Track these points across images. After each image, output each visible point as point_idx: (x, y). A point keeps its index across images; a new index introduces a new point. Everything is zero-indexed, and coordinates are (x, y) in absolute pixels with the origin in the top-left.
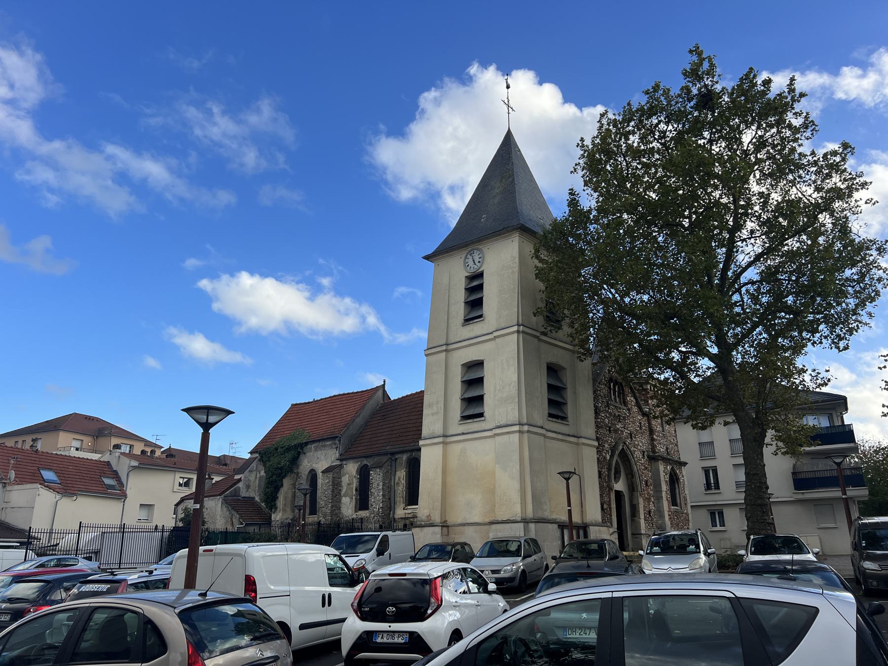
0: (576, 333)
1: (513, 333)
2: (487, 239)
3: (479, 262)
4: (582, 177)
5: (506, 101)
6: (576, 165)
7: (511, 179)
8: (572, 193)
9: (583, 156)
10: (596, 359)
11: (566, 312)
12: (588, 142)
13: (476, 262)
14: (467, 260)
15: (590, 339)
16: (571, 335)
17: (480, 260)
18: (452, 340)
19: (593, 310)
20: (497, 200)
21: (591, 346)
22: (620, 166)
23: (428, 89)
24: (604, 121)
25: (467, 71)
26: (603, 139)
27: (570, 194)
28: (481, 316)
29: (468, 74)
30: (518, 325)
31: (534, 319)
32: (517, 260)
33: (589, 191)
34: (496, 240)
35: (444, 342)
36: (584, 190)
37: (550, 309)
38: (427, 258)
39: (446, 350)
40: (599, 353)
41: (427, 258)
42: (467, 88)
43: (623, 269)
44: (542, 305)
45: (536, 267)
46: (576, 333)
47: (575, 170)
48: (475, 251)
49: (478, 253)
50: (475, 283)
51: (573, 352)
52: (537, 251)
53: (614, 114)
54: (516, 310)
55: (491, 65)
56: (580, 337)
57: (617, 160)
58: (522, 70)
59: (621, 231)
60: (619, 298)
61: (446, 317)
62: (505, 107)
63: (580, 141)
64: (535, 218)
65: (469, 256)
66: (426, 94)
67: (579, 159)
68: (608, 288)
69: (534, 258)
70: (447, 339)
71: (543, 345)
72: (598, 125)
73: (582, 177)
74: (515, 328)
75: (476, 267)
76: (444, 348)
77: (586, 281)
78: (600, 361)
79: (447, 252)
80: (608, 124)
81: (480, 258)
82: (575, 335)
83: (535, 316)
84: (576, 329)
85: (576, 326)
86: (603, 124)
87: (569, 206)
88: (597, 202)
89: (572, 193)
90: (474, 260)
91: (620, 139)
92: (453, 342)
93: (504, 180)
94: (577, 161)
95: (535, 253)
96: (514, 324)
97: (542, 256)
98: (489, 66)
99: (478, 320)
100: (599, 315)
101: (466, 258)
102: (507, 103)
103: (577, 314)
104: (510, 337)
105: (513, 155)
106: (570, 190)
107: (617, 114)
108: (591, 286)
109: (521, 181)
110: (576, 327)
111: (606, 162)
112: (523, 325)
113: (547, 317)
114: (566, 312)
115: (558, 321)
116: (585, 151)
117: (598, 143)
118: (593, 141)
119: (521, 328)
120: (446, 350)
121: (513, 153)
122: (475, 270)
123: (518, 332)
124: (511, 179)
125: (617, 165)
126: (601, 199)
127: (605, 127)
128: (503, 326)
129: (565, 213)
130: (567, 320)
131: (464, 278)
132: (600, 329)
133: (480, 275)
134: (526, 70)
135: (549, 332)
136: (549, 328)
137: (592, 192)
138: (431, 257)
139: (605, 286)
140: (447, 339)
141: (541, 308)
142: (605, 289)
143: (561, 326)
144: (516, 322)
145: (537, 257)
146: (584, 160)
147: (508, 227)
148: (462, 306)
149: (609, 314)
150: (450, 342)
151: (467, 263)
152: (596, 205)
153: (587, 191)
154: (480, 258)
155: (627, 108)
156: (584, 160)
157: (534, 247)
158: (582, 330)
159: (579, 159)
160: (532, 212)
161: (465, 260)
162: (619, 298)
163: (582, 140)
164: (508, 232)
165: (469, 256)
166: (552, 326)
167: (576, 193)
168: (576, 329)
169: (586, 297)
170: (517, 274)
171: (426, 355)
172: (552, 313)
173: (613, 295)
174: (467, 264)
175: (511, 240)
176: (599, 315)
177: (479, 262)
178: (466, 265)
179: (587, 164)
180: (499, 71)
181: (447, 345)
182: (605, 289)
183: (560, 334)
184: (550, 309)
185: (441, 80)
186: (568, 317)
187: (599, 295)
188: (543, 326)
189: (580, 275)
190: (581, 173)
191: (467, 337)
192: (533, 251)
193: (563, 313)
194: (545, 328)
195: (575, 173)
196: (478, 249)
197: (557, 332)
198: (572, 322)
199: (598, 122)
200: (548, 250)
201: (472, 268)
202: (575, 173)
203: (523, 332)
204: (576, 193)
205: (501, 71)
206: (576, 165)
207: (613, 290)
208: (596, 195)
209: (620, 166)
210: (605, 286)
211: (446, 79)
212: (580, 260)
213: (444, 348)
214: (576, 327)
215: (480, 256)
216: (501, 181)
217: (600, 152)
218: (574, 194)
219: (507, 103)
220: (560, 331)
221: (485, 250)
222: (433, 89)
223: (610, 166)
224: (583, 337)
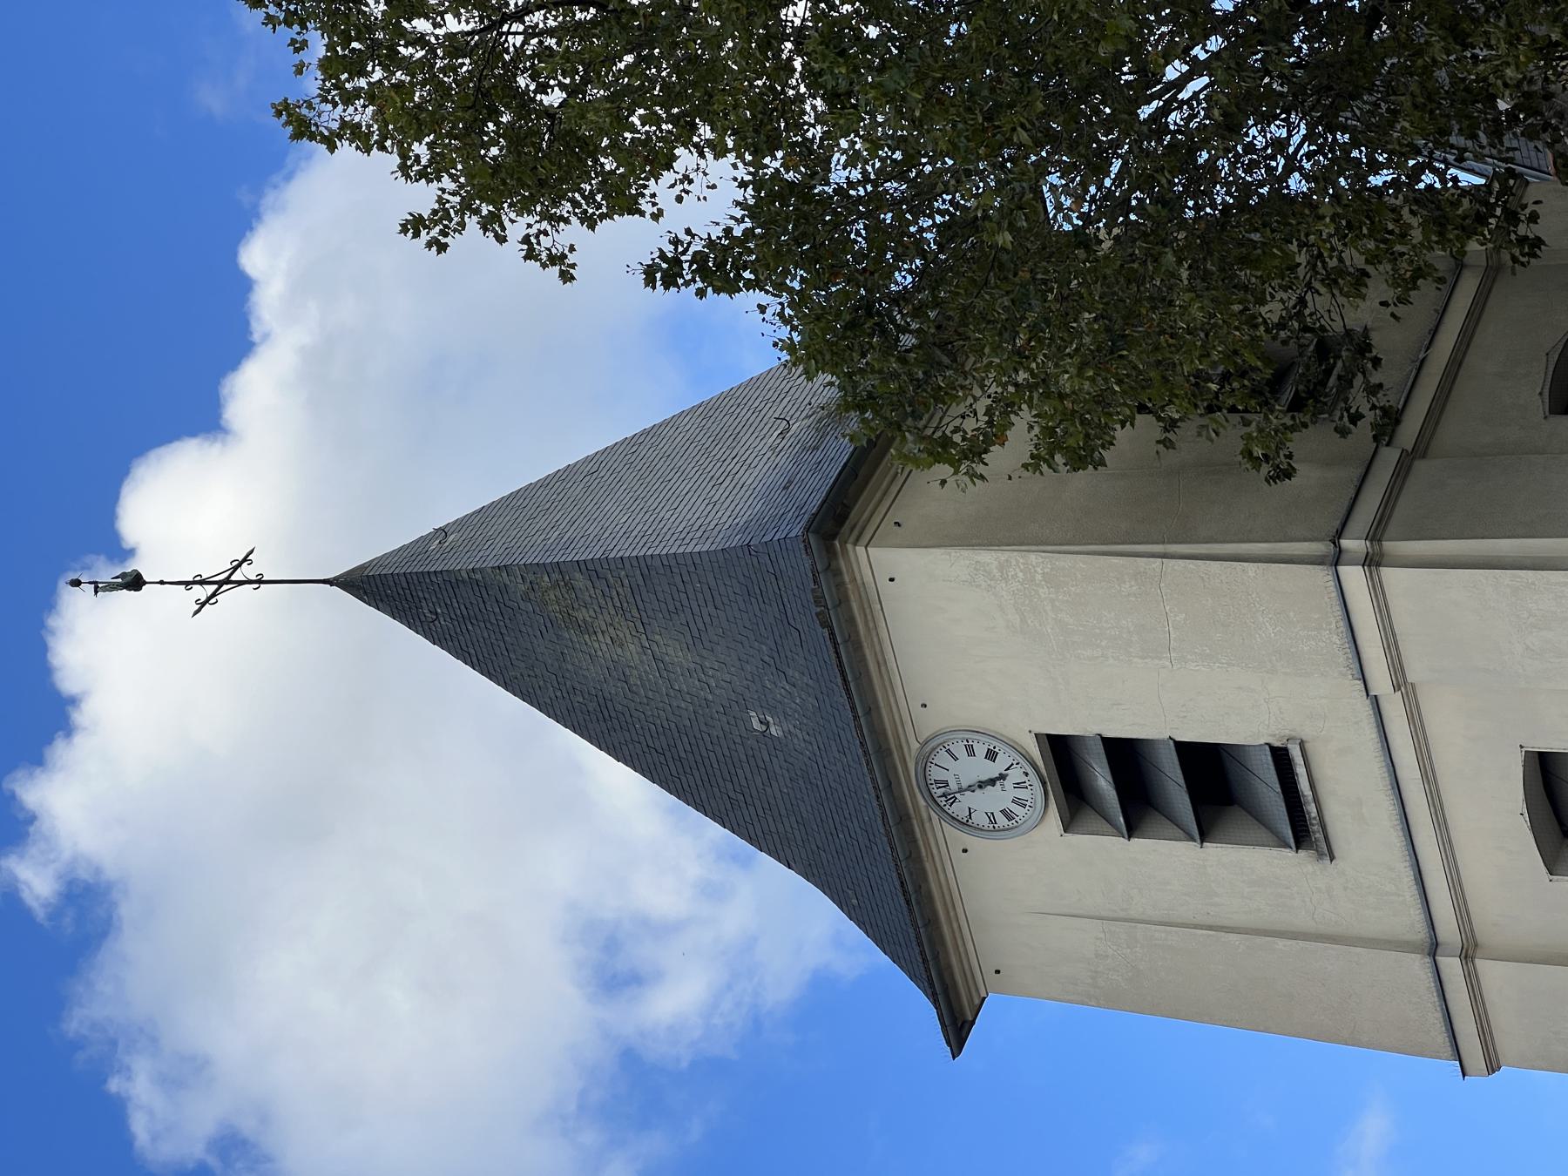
0: (1395, 258)
1: (1378, 591)
2: (872, 709)
3: (991, 755)
4: (592, 227)
5: (201, 592)
6: (531, 255)
7: (580, 581)
8: (664, 272)
9: (491, 224)
10: (1533, 156)
11: (1272, 311)
12: (423, 197)
13: (993, 770)
14: (980, 819)
15: (1430, 187)
16: (1406, 285)
17: (981, 750)
18: (1410, 922)
19: (1270, 170)
20: (677, 655)
21: (1466, 179)
22: (551, 42)
23: (115, 1112)
24: (330, 117)
25: (40, 914)
26: (414, 123)
27: (670, 281)
28: (1281, 757)
29: (56, 914)
30: (1336, 560)
31: (1307, 476)
32: (989, 558)
33: (661, 188)
34: (882, 663)
35: (1418, 966)
36: (656, 217)
37: (1255, 392)
38: (957, 1029)
39: (1468, 955)
40: (1508, 140)
41: (957, 1029)
42: (127, 911)
43: (1329, 76)
44: (1232, 434)
45: (1036, 462)
46: (1395, 258)
47: (556, 259)
48: (935, 774)
49: (942, 758)
50: (1102, 780)
51: (1492, 274)
52: (940, 450)
53: (300, 69)
54: (1252, 568)
55: (13, 797)
56: (1417, 235)
57: (519, 51)
58: (51, 641)
59: (872, 32)
60: (1215, 43)
61: (1281, 944)
62: (228, 597)
63: (416, 235)
64: (782, 460)
65: (959, 810)
66: (140, 1126)
67: (501, 239)
68: (1158, 96)
69: (980, 469)
70: (1400, 946)
71: (1450, 432)
72: (346, 149)
73: (592, 227)
74: (1354, 576)
75: (1015, 775)
76: (1451, 966)
77: (1114, 206)
78: (1547, 137)
79: (932, 922)
80: (349, 98)
81: (970, 751)
82: (1403, 265)
83: (1288, 474)
84: (1373, 259)
85: (1354, 258)
86: (344, 124)
87: (730, 287)
88: (720, 152)
89: (664, 272)
90: (982, 784)
91: (419, 40)
92: (1416, 914)
93: (582, 615)
94: (514, 248)
95: (955, 464)
96: (1332, 584)
97: (970, 425)
98: (22, 808)
99: (1300, 770)
100: (1296, 139)
101: (965, 824)
102: (211, 589)
103: (1288, 256)
104: (1398, 605)
105: (459, 563)
106: (650, 281)
107: (297, 58)
108: (1143, 182)
109: (593, 530)
110: (1360, 261)
111: (523, 104)
112: (1340, 534)
113: (1296, 405)
114: (1272, 311)
115: (1325, 350)
116: (466, 207)
117: (430, 146)
118: (422, 175)
119: (1353, 544)
120: (1468, 955)
121: (452, 565)
122: (1033, 778)
123: (1372, 562)
124: (580, 581)
125: (544, 53)
126: (706, 132)
127: (363, 115)
128: (1336, 638)
129: (762, 309)
130: (1319, 301)
131: (1069, 837)
132: (1373, 134)
133: (1061, 750)
134: (52, 622)
135: (1381, 400)
136: (1359, 400)
137: (668, 177)
138: (954, 1019)
139: (1145, 112)
140: (1400, 946)
141: (1248, 438)
142: (1164, 111)
143: (1348, 333)
144: (1320, 576)
145: (976, 450)
146: (508, 214)
147: (819, 600)
148: (1217, 855)
149: (1298, 92)
150: (1420, 933)
151: (992, 818)
152: (731, 157)
153: (665, 197)
154: (970, 751)
155: (272, 10)
156: (508, 214)
157: (917, 463)
158: (1375, 232)
159: (501, 239)
160: (749, 478)
161: (977, 830)
162: (1215, 43)
163: (414, 225)
164: (843, 601)
165: (959, 810)
166: (1346, 382)
167: (669, 250)
168: (1373, 259)
169: (1197, 208)
170: (1065, 562)
171: (1492, 1067)
172: (1277, 383)
173: (1196, 69)
174: (1002, 821)
175: (883, 582)
176: (1296, 139)
177: (991, 755)
178: (1003, 826)
179: (533, 200)
180: (68, 683)
181: (1433, 948)
182: (1164, 111)
183: (1390, 341)
184: (1255, 392)
185: (77, 1045)
186: (1302, 302)
187: (1191, 142)
188: (1343, 432)
189: (1081, 239)
190: (572, 233)
191: (1396, 838)
192: (944, 470)
193: (1282, 325)
194: (1355, 418)
195: (571, 259)
196: (925, 761)
197: (1376, 362)
198: (1331, 281)
199: (332, 148)
200: (943, 397)
201: (1021, 793)
202: (571, 259)
203: (1376, 534)
204: (669, 250)
205: (49, 741)
206: (531, 255)
207: (1171, 73)
208: (685, 159)
209: (551, 42)
210: (1145, 112)
211: (74, 1024)
212: (1005, 239)
213: (1451, 966)
214: (1360, 261)
215: (959, 750)
216: (585, 628)
217: (472, 137)
218: (676, 262)
219: (211, 589)
220: (1375, 338)
221: (929, 723)
222: (114, 1085)
223: (543, 88)
224: (1414, 221)
